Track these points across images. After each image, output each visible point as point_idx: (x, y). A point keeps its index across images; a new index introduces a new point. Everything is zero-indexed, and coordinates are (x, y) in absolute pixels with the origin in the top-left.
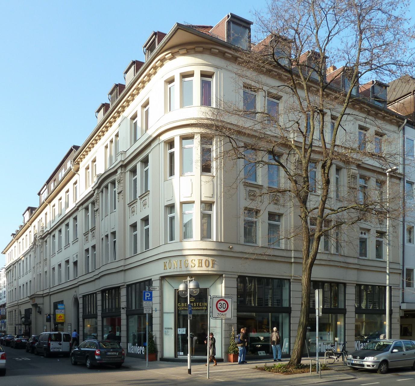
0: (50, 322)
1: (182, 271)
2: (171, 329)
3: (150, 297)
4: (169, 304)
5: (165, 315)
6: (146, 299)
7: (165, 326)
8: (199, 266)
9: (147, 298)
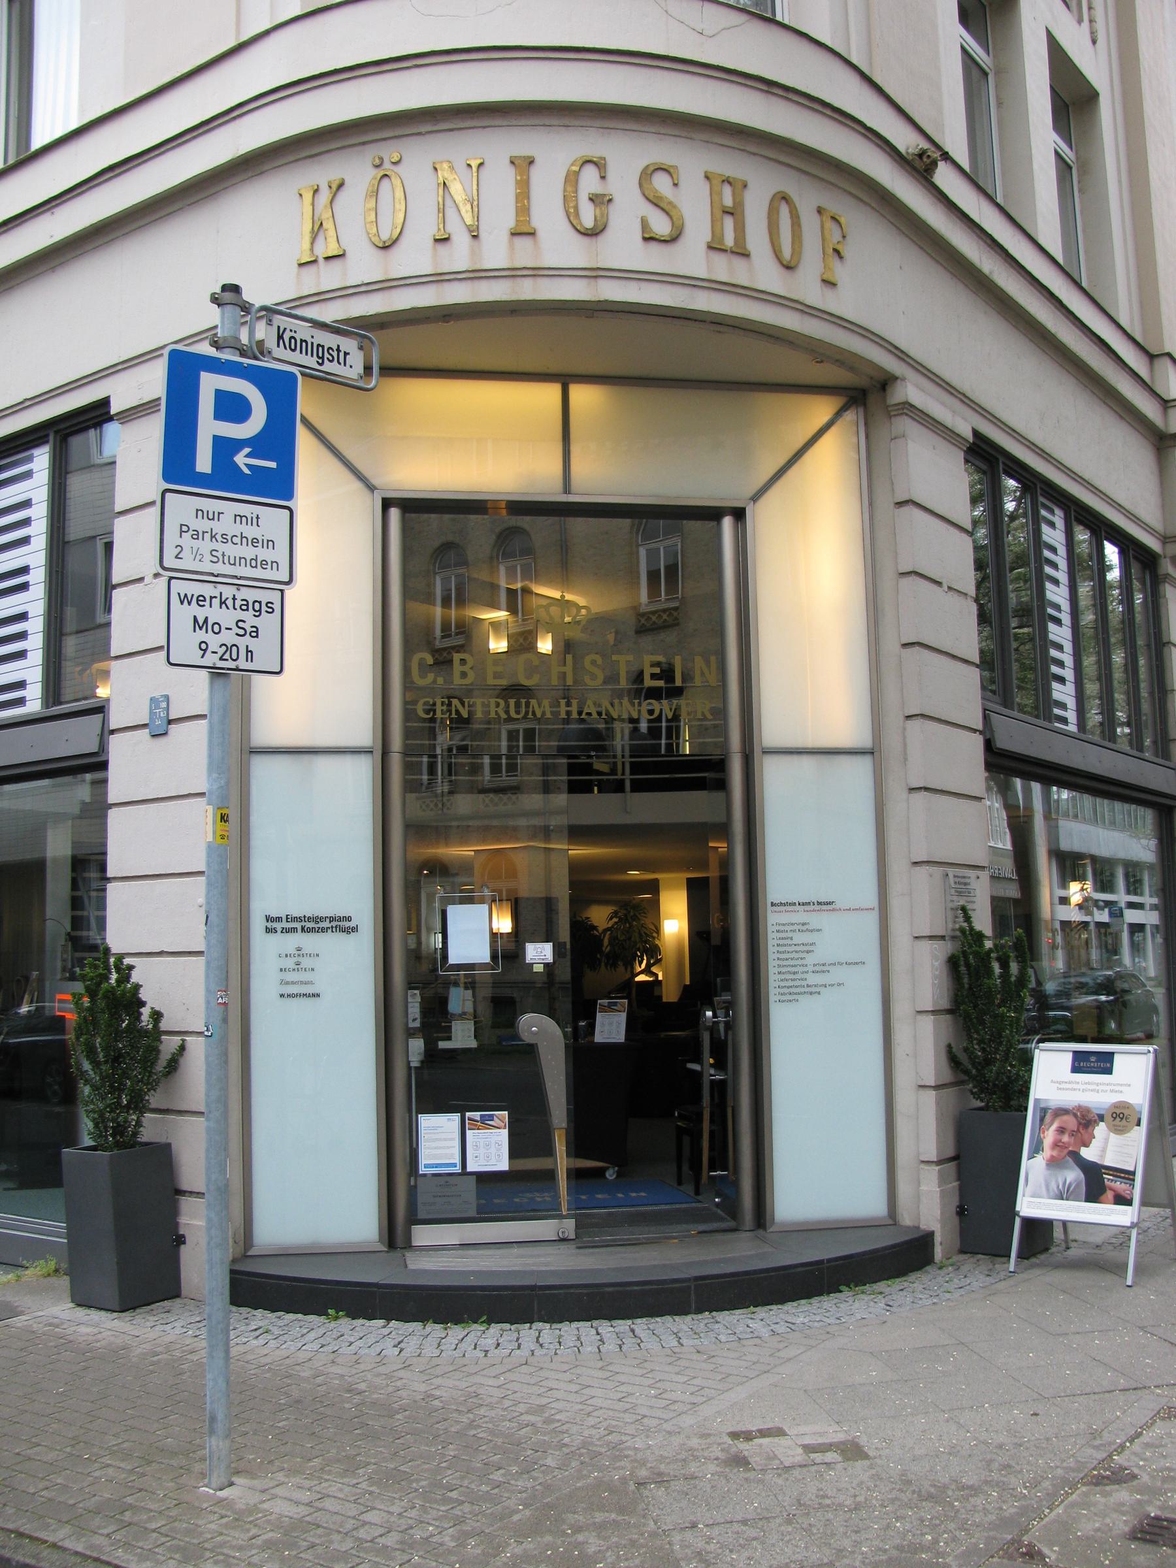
0: (1113, 1053)
1: (536, 272)
2: (341, 925)
3: (258, 445)
4: (326, 665)
5: (267, 776)
6: (204, 463)
7: (263, 904)
8: (715, 247)
9: (224, 448)
